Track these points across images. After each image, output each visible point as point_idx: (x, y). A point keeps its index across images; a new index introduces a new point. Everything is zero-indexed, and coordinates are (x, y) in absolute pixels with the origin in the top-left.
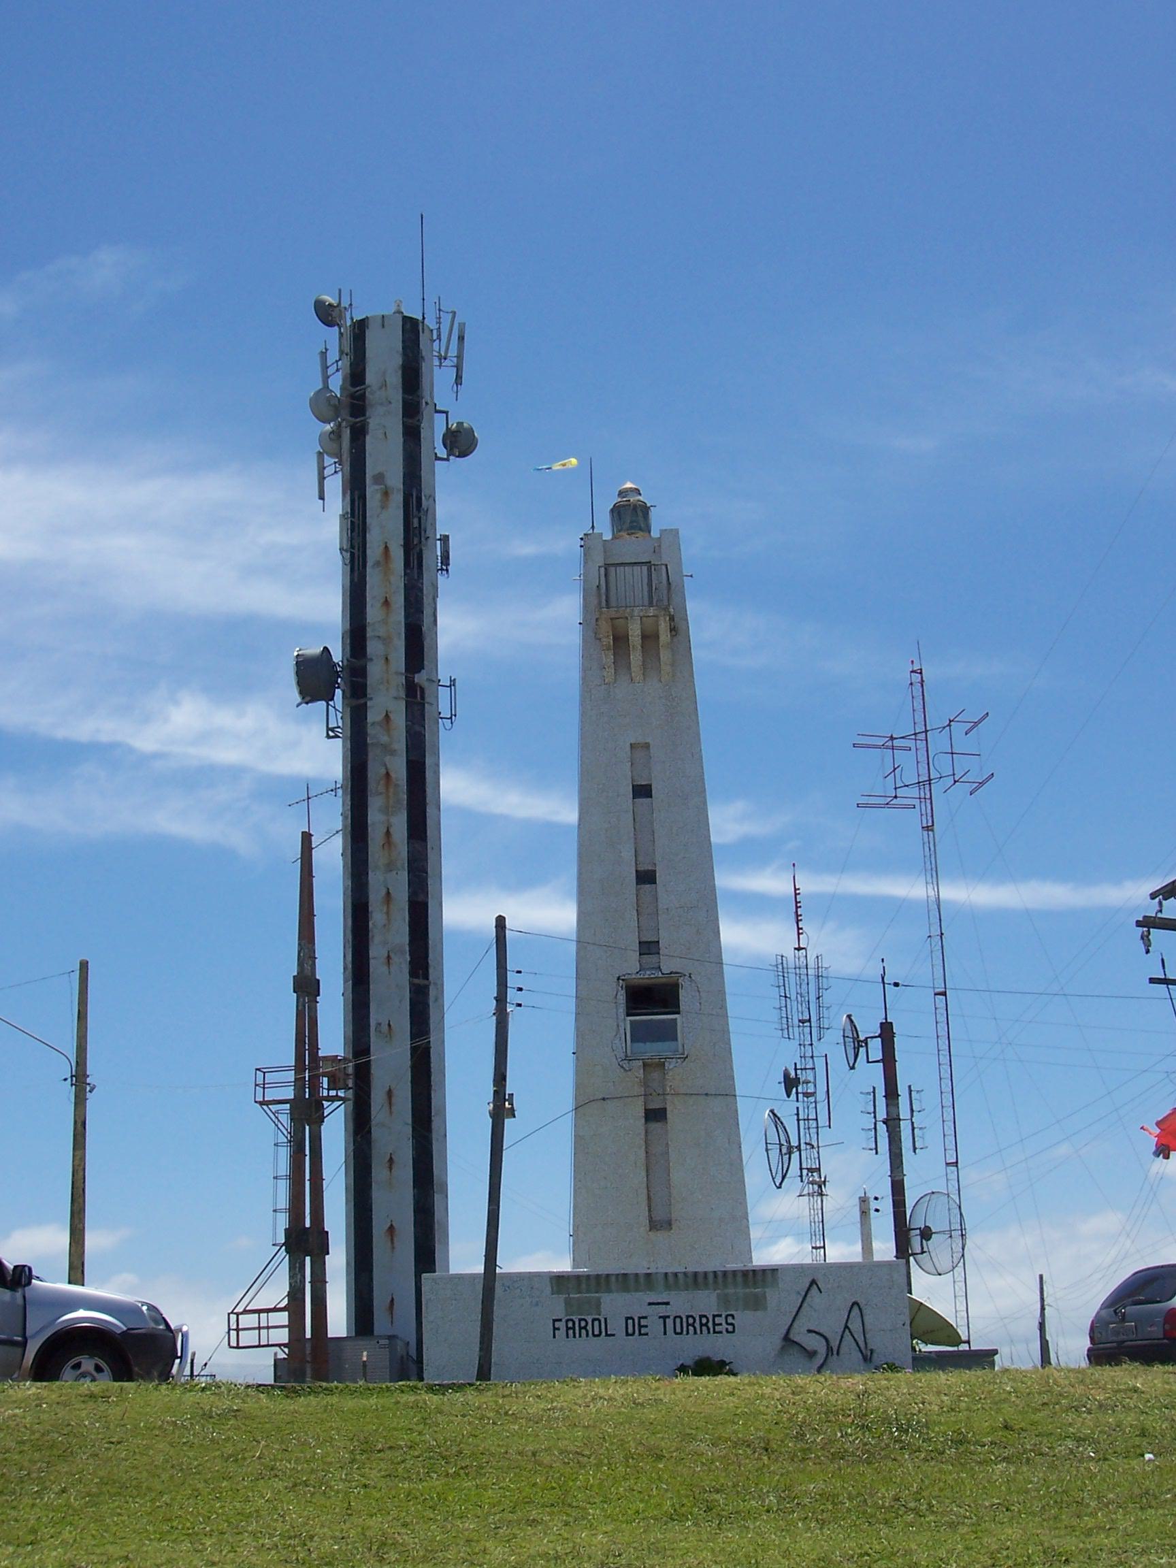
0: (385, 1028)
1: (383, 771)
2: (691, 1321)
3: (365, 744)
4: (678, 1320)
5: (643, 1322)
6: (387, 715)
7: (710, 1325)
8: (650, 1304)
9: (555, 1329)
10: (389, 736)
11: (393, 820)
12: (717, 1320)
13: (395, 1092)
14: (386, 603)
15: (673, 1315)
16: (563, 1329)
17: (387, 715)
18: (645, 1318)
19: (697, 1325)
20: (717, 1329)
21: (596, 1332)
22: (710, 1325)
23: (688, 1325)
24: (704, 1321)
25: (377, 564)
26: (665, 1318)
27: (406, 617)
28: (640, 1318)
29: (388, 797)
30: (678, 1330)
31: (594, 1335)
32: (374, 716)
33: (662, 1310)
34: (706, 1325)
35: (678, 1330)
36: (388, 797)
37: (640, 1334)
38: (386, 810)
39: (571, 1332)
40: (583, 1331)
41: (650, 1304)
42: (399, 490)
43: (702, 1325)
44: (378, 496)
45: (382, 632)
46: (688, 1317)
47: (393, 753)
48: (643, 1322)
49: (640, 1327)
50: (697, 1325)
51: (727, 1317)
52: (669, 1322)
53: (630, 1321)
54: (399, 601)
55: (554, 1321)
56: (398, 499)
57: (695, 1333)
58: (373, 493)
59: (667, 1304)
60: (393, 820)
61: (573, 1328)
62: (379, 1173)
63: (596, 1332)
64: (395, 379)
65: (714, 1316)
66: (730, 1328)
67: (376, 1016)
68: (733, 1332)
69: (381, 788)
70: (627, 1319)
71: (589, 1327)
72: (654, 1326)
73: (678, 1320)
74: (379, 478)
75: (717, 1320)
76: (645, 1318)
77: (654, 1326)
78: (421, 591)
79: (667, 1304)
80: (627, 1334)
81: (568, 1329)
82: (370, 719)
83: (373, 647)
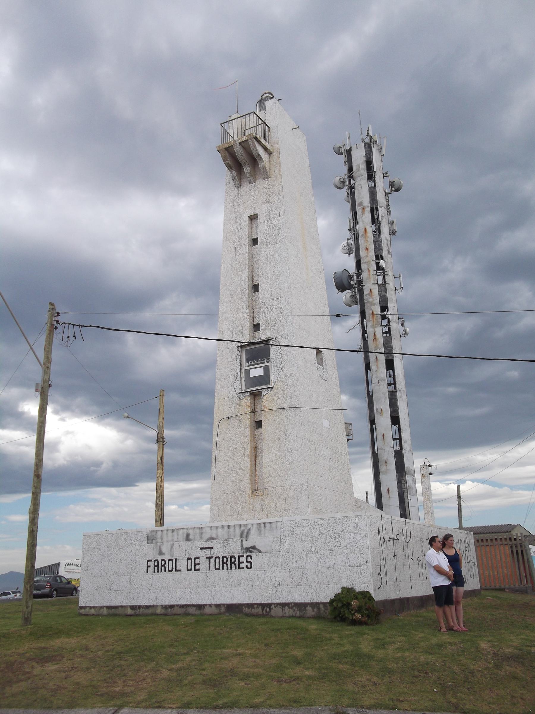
0: (380, 410)
1: (371, 312)
2: (225, 560)
3: (364, 303)
4: (217, 560)
5: (197, 561)
6: (371, 291)
7: (237, 563)
8: (201, 549)
9: (148, 567)
10: (373, 298)
11: (376, 329)
12: (242, 559)
13: (385, 435)
14: (367, 249)
15: (215, 556)
16: (152, 567)
17: (371, 291)
18: (198, 558)
19: (229, 563)
20: (241, 565)
21: (170, 569)
22: (237, 563)
23: (223, 563)
24: (233, 560)
25: (363, 235)
26: (210, 558)
27: (375, 253)
28: (195, 558)
29: (374, 322)
30: (217, 567)
31: (169, 571)
32: (366, 292)
33: (209, 553)
34: (234, 563)
35: (217, 567)
36: (374, 322)
37: (195, 570)
38: (373, 326)
39: (156, 568)
40: (163, 568)
41: (201, 549)
42: (368, 207)
43: (231, 563)
44: (361, 211)
45: (366, 260)
46: (223, 557)
47: (374, 304)
48: (197, 561)
49: (195, 564)
50: (229, 563)
51: (247, 557)
52: (212, 561)
53: (190, 561)
54: (372, 247)
55: (148, 561)
56: (368, 210)
57: (227, 569)
58: (359, 210)
59: (211, 548)
60: (376, 329)
61: (158, 566)
62: (382, 468)
63: (170, 569)
64: (363, 166)
65: (239, 557)
66: (249, 565)
67: (376, 406)
68: (251, 568)
69: (371, 319)
70: (188, 559)
71: (167, 565)
72: (203, 564)
73: (217, 560)
74: (361, 204)
75: (242, 559)
76: (198, 558)
77: (203, 564)
78: (381, 242)
79: (211, 548)
80: (188, 570)
81: (155, 566)
82: (365, 294)
83: (363, 266)
